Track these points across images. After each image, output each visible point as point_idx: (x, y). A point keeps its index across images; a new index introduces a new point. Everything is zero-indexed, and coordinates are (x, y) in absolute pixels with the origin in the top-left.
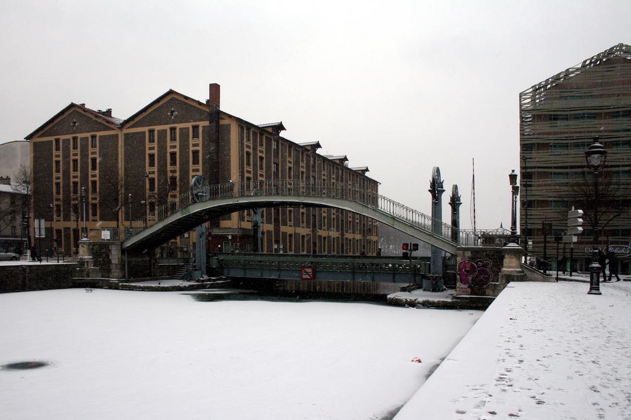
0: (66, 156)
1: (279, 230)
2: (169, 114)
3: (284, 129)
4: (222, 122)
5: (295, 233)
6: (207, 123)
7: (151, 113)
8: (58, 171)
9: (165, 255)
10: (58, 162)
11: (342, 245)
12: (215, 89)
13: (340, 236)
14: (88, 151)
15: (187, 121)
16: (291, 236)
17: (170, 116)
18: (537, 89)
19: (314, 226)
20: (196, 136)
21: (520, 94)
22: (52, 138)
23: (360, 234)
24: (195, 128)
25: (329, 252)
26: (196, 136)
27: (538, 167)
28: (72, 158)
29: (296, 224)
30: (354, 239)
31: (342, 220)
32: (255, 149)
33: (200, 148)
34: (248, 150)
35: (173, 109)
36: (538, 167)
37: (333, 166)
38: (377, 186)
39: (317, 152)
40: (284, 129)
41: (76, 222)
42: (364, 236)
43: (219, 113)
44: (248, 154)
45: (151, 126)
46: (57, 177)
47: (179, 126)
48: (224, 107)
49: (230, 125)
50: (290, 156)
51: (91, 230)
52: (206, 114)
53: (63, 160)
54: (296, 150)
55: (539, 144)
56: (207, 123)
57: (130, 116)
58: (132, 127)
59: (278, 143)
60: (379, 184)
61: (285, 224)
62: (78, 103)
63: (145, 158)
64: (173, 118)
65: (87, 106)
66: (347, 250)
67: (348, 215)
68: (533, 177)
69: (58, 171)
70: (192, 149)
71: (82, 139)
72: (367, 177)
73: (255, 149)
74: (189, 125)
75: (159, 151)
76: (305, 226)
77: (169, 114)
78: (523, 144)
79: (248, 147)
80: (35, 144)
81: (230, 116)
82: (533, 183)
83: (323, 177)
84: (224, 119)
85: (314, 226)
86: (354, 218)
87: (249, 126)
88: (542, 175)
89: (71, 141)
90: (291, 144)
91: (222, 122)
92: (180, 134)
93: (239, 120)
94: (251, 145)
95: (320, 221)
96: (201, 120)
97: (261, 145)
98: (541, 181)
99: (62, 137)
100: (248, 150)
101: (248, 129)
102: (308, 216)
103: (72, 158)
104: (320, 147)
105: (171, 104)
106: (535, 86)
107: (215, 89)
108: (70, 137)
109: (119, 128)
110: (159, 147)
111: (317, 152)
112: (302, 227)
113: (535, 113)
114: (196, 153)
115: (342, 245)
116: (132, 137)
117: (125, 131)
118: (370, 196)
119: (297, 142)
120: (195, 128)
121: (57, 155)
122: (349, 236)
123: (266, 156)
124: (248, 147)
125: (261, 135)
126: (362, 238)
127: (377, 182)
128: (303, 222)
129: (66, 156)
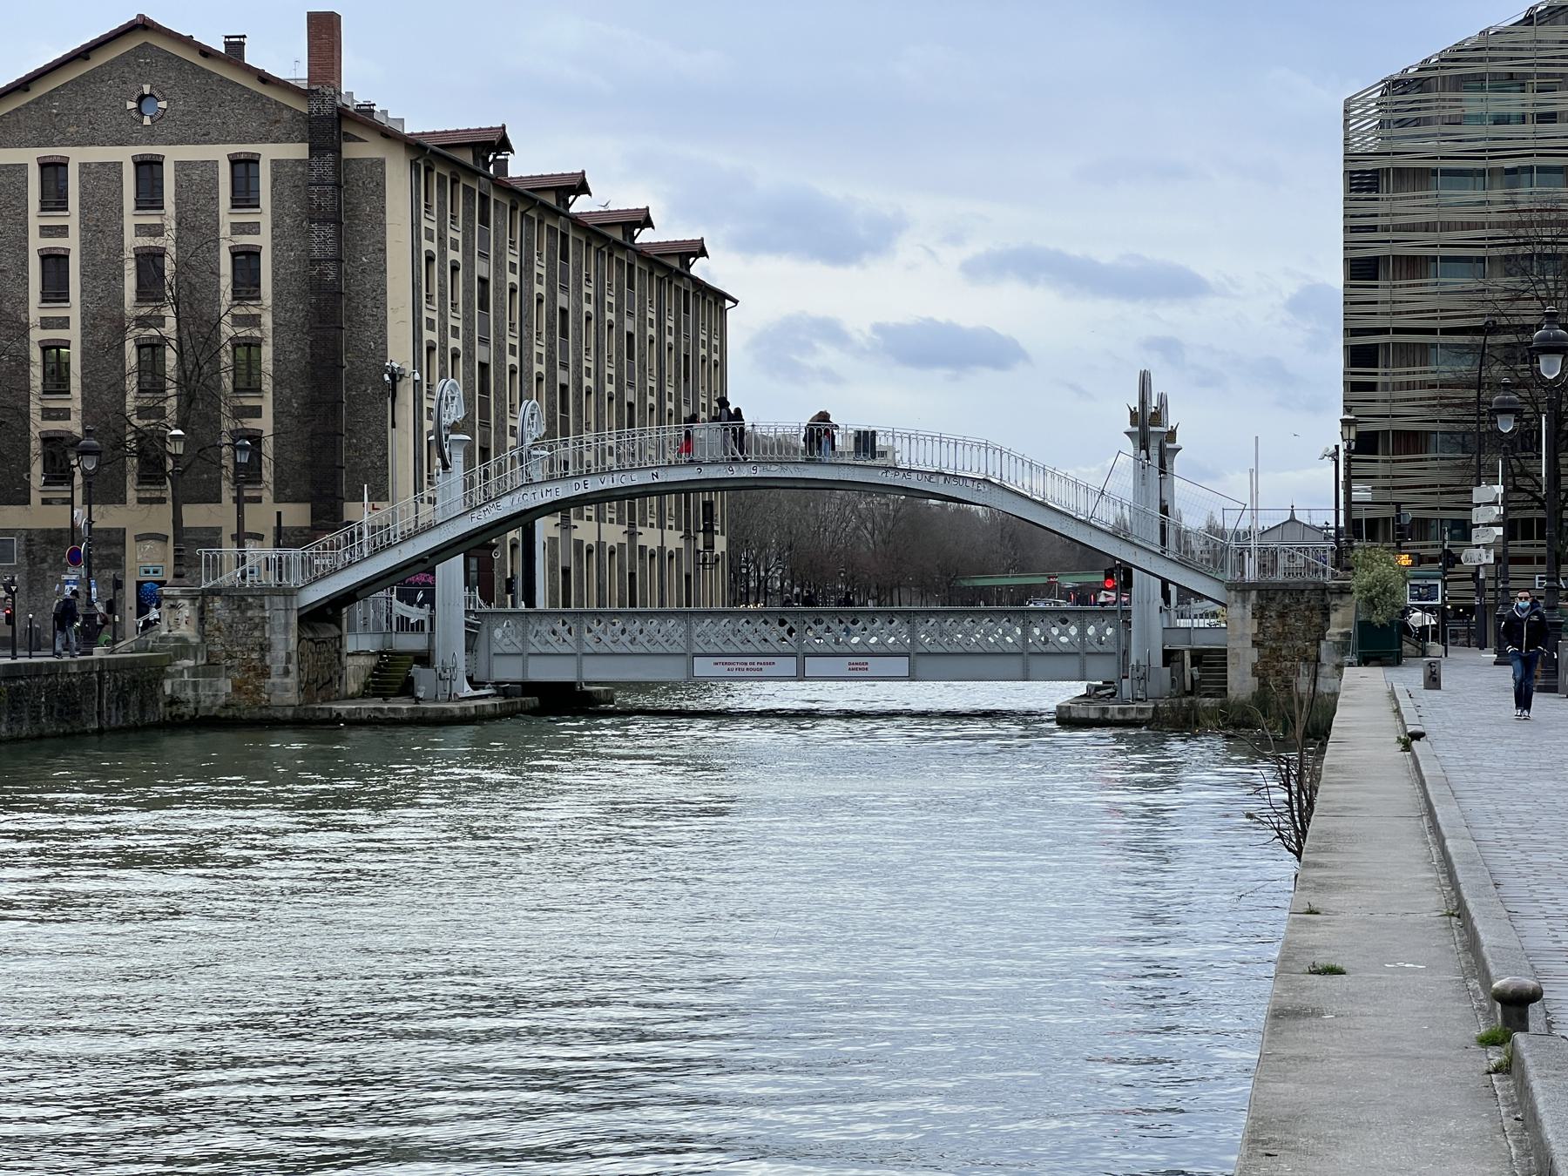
6: (299, 151)
9: (415, 614)
11: (632, 575)
15: (204, 139)
17: (134, 115)
20: (244, 197)
21: (1348, 102)
24: (244, 167)
25: (662, 604)
26: (244, 197)
27: (1397, 331)
35: (147, 89)
36: (1397, 331)
38: (723, 311)
39: (694, 271)
41: (247, 529)
45: (50, 143)
47: (172, 155)
49: (382, 162)
51: (140, 538)
55: (1399, 172)
56: (299, 151)
60: (728, 303)
63: (25, 264)
64: (147, 121)
66: (580, 595)
67: (504, 421)
68: (1381, 272)
72: (696, 282)
74: (220, 154)
75: (84, 243)
77: (131, 105)
78: (1352, 260)
81: (390, 135)
82: (1379, 379)
84: (361, 140)
88: (1408, 354)
91: (351, 151)
96: (264, 139)
110: (85, 227)
111: (694, 271)
120: (244, 167)
122: (649, 538)
127: (724, 296)
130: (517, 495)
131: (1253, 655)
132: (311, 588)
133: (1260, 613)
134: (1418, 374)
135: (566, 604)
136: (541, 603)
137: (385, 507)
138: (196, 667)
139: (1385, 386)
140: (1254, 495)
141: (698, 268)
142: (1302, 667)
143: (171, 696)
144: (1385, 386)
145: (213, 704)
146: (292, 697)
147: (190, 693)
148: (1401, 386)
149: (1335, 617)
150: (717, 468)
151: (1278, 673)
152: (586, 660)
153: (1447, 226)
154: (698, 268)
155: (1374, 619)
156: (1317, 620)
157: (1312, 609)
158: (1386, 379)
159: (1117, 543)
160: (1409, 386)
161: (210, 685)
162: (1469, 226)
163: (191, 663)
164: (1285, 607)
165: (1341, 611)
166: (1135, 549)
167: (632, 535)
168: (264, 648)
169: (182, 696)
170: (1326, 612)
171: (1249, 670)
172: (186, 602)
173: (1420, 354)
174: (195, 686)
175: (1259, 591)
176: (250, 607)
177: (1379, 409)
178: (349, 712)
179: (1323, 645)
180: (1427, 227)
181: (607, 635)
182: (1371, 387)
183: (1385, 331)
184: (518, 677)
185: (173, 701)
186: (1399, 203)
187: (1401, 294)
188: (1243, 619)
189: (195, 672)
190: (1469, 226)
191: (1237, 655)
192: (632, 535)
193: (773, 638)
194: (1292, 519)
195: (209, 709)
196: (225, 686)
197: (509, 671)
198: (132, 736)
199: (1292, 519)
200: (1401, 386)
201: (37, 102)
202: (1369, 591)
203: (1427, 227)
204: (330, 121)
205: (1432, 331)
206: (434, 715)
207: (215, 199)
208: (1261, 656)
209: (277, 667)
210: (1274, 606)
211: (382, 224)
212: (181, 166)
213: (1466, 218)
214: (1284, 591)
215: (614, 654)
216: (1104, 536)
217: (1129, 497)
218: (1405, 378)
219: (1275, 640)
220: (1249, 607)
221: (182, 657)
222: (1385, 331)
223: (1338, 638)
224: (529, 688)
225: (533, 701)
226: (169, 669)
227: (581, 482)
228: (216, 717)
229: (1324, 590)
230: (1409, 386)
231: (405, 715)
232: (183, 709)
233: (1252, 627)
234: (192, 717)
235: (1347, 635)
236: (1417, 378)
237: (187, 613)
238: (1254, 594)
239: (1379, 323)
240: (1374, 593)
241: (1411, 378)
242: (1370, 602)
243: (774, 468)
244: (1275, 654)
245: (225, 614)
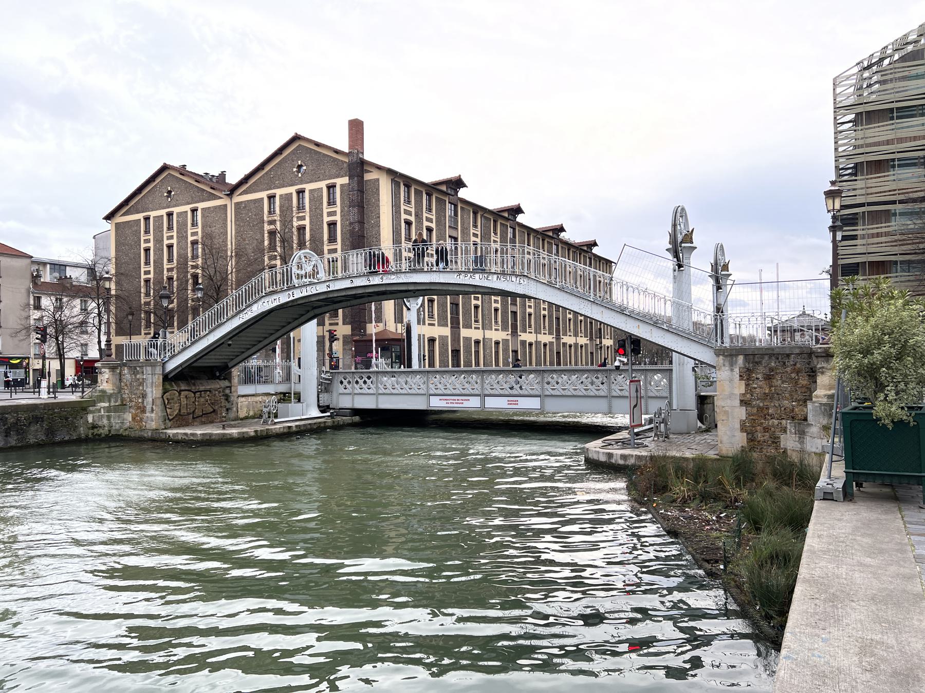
0: (159, 241)
1: (459, 335)
2: (295, 170)
3: (464, 185)
4: (368, 177)
5: (484, 339)
6: (345, 180)
7: (270, 170)
8: (147, 263)
10: (147, 250)
11: (558, 353)
12: (356, 127)
13: (554, 340)
14: (186, 232)
16: (477, 342)
18: (865, 69)
19: (514, 327)
21: (835, 80)
22: (140, 216)
23: (586, 336)
27: (870, 204)
28: (166, 242)
29: (537, 332)
30: (576, 344)
31: (558, 319)
32: (418, 216)
33: (338, 218)
34: (408, 217)
35: (300, 163)
36: (870, 204)
37: (543, 240)
39: (593, 251)
40: (464, 185)
42: (514, 333)
43: (363, 163)
44: (408, 223)
45: (271, 189)
46: (147, 272)
48: (370, 154)
49: (378, 180)
50: (475, 226)
52: (345, 165)
53: (155, 246)
54: (486, 218)
55: (868, 113)
56: (345, 180)
57: (242, 176)
58: (245, 192)
59: (514, 229)
61: (468, 326)
62: (177, 164)
65: (188, 169)
69: (147, 263)
70: (326, 219)
71: (179, 214)
73: (418, 216)
74: (323, 185)
76: (436, 323)
77: (295, 170)
79: (408, 213)
80: (118, 225)
81: (379, 168)
83: (473, 239)
85: (514, 327)
86: (537, 306)
87: (409, 182)
88: (876, 217)
89: (165, 218)
90: (477, 209)
92: (310, 199)
93: (390, 172)
94: (413, 210)
95: (524, 319)
96: (338, 176)
97: (475, 226)
98: (874, 228)
99: (153, 214)
100: (475, 239)
101: (408, 186)
102: (505, 313)
103: (166, 242)
104: (523, 212)
105: (296, 156)
106: (862, 62)
107: (356, 127)
108: (163, 212)
109: (227, 195)
111: (593, 251)
112: (496, 330)
113: (860, 109)
114: (332, 225)
115: (558, 353)
116: (245, 207)
117: (237, 199)
118: (600, 282)
119: (535, 227)
120: (331, 187)
121: (147, 241)
122: (569, 340)
123: (437, 225)
124: (408, 213)
125: (429, 195)
126: (588, 342)
128: (496, 322)
129: (159, 241)
130: (260, 303)
131: (741, 413)
132: (171, 362)
133: (747, 375)
134: (883, 228)
135: (432, 364)
136: (415, 365)
137: (381, 325)
138: (110, 406)
139: (863, 237)
140: (761, 291)
141: (595, 250)
142: (787, 423)
143: (93, 424)
144: (863, 237)
145: (121, 428)
146: (153, 425)
147: (105, 421)
148: (873, 236)
149: (822, 380)
150: (361, 279)
151: (766, 430)
152: (380, 397)
153: (901, 140)
154: (595, 250)
155: (880, 410)
156: (804, 381)
157: (798, 372)
158: (864, 232)
159: (623, 318)
160: (878, 235)
161: (119, 417)
162: (915, 138)
163: (107, 405)
164: (771, 370)
165: (828, 374)
166: (638, 323)
167: (558, 338)
168: (144, 396)
169: (100, 423)
170: (812, 374)
171: (738, 426)
172: (107, 370)
173: (887, 216)
174: (109, 418)
175: (746, 356)
176: (138, 373)
177: (860, 249)
178: (174, 435)
179: (810, 406)
180: (888, 142)
181: (438, 383)
182: (854, 237)
183: (862, 205)
184: (349, 406)
185: (94, 427)
186: (870, 181)
187: (871, 183)
188: (731, 380)
189: (108, 409)
190: (915, 138)
191: (726, 413)
192: (558, 338)
193: (506, 386)
194: (804, 313)
195: (118, 430)
196: (128, 417)
197: (346, 402)
198: (14, 454)
199: (804, 313)
200: (873, 236)
201: (266, 173)
202: (866, 352)
203: (888, 142)
204: (358, 167)
205: (894, 202)
206: (217, 438)
207: (322, 203)
208: (749, 414)
209: (149, 408)
210: (761, 369)
211: (379, 206)
212: (311, 191)
213: (912, 135)
214: (771, 356)
215: (392, 394)
216: (613, 314)
217: (670, 296)
218: (875, 231)
219: (763, 400)
220: (737, 370)
221: (101, 401)
222: (862, 205)
223: (825, 400)
224: (356, 412)
225: (357, 419)
226: (91, 408)
227: (291, 293)
228: (121, 435)
229: (810, 354)
230: (878, 235)
231: (199, 438)
232: (101, 431)
233: (740, 388)
234: (107, 435)
235: (831, 397)
236: (884, 230)
237: (107, 376)
238: (741, 359)
239: (859, 200)
240: (877, 356)
241: (879, 230)
242: (870, 374)
243: (393, 277)
244: (762, 412)
245: (128, 376)
